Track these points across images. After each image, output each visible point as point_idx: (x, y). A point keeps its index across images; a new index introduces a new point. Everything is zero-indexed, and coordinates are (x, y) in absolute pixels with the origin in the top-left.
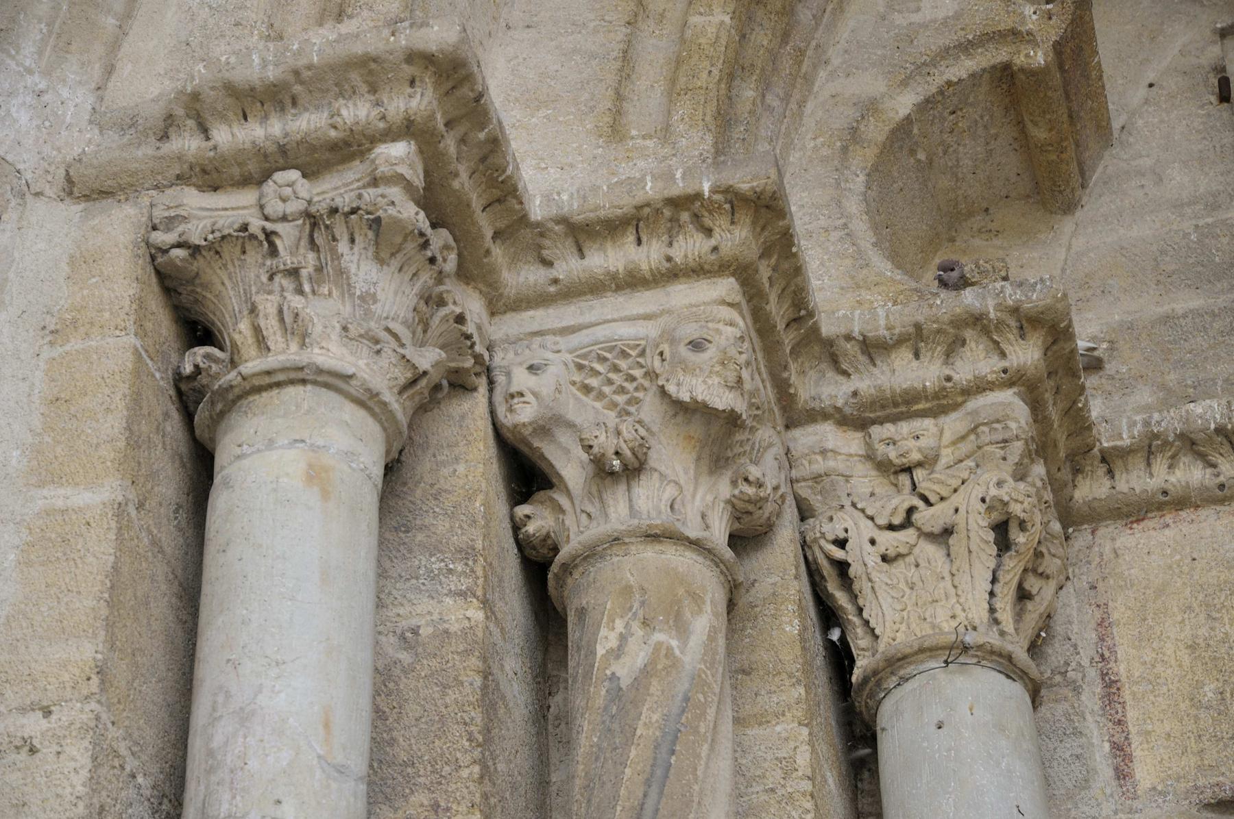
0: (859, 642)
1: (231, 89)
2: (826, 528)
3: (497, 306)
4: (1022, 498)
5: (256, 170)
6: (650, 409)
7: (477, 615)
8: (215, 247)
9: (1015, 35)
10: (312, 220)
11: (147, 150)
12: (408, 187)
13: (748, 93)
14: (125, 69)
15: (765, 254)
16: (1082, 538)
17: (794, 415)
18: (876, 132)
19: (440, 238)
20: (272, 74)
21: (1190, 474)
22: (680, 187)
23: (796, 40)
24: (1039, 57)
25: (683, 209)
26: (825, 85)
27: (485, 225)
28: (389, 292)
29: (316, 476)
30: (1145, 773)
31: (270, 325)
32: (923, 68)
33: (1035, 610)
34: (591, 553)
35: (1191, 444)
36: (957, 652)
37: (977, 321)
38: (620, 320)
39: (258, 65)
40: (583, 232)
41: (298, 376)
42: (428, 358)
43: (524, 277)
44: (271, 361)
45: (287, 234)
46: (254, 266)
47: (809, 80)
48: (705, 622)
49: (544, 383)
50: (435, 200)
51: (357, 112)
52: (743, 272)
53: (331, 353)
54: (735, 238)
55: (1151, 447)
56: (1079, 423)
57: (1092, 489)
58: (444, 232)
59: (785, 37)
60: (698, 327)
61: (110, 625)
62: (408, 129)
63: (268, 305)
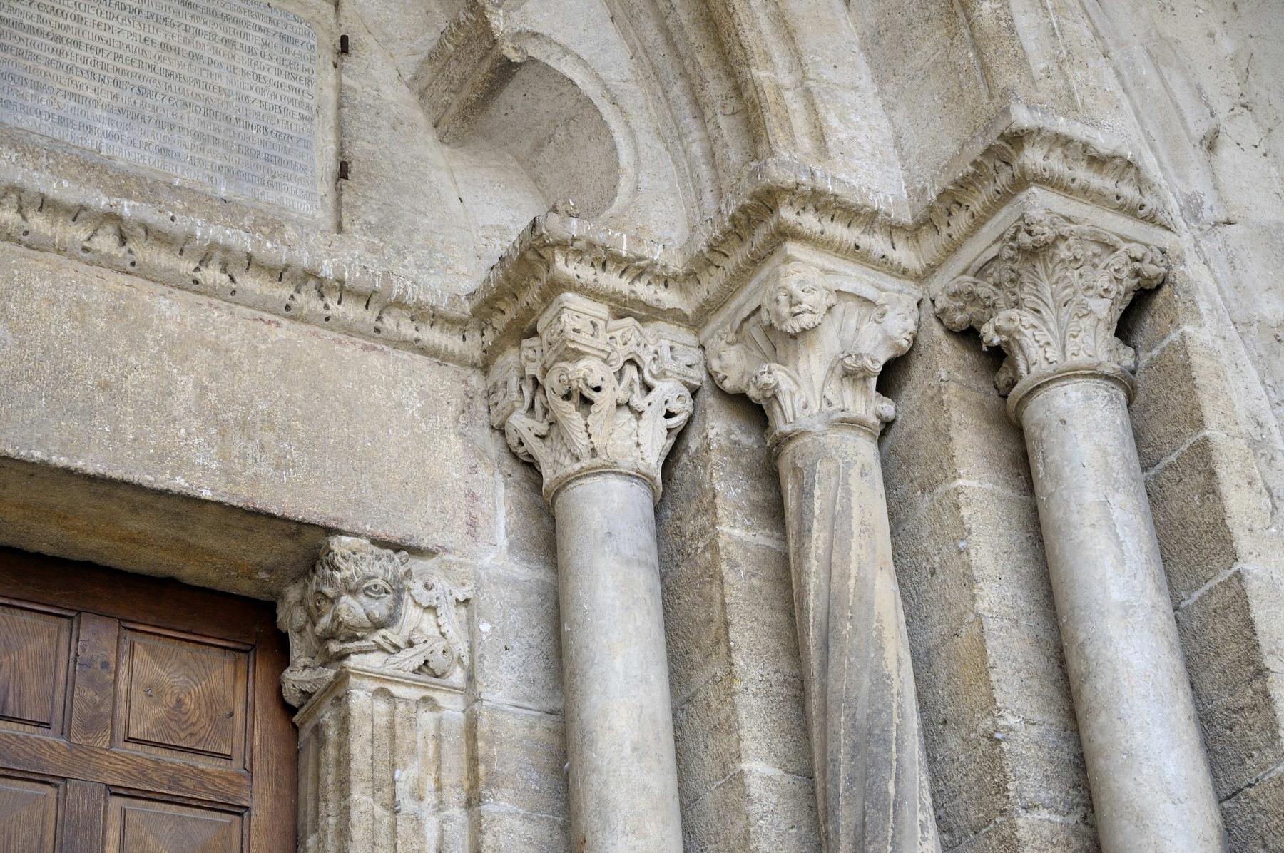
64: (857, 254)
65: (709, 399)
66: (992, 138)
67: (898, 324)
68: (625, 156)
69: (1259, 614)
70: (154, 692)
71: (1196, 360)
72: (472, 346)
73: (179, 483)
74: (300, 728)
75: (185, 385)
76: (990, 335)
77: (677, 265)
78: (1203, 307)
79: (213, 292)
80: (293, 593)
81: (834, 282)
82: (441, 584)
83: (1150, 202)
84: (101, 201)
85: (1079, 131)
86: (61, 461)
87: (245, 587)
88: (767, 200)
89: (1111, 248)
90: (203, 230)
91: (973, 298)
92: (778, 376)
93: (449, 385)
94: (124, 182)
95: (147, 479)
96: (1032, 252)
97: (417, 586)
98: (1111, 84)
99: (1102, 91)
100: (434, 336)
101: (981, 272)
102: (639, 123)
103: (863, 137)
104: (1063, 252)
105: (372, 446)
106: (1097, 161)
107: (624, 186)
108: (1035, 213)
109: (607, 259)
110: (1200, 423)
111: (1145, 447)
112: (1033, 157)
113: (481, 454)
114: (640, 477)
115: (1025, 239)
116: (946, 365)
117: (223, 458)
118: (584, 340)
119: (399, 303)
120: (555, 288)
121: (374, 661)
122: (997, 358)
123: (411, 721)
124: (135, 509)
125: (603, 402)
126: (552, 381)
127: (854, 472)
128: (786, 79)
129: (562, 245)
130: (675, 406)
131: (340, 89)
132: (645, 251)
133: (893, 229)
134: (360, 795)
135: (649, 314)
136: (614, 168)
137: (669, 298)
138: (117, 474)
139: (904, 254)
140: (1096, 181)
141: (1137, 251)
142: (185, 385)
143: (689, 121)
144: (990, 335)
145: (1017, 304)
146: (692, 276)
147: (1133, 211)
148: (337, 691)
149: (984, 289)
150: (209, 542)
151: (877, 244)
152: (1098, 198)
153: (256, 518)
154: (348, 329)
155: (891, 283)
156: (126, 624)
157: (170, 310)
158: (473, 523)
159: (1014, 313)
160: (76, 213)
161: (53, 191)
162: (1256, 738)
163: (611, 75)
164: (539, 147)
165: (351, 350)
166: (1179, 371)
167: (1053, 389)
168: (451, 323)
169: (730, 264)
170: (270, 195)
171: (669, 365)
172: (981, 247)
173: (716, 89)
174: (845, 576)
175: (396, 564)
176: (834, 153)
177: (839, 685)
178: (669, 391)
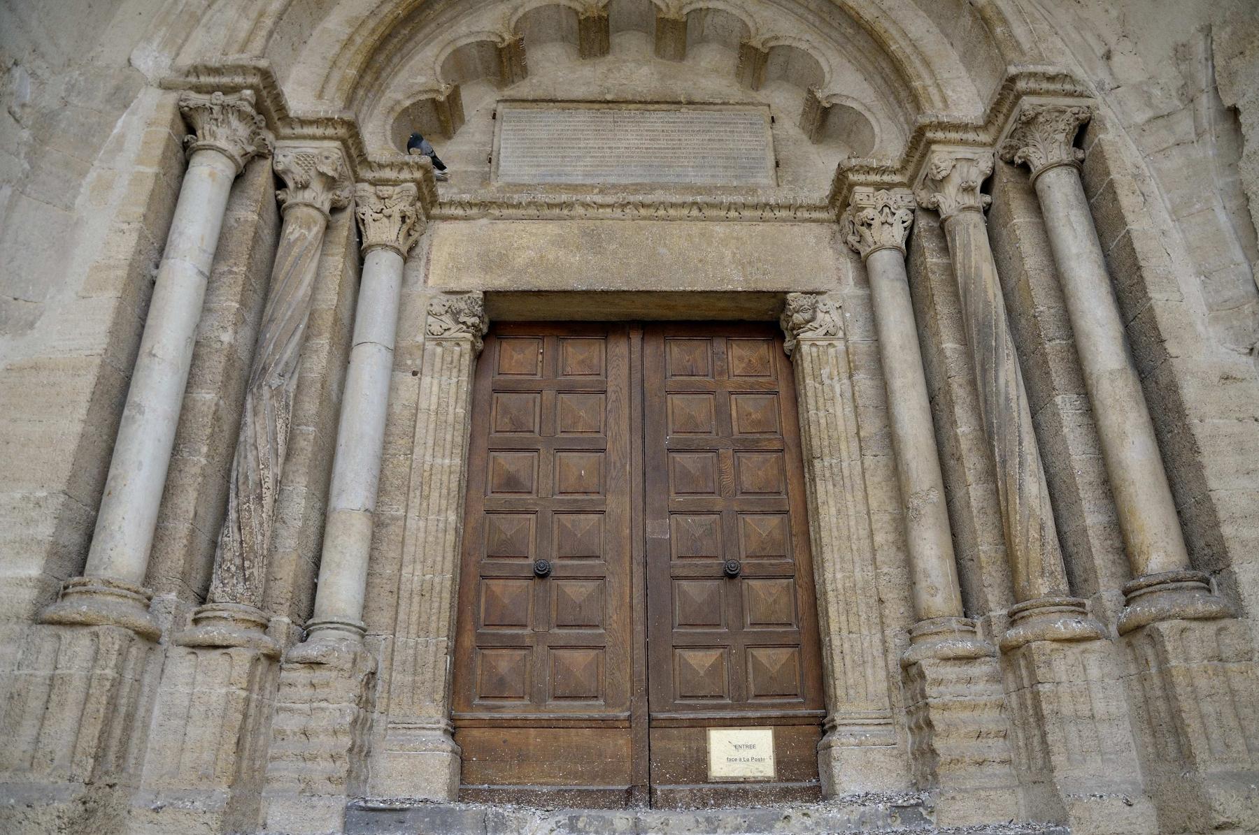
0: (364, 240)
1: (206, 67)
2: (361, 210)
3: (278, 137)
4: (410, 211)
5: (210, 90)
6: (313, 173)
7: (256, 217)
8: (197, 109)
9: (438, 91)
10: (223, 107)
11: (181, 79)
12: (250, 103)
13: (361, 92)
14: (182, 55)
15: (351, 137)
16: (431, 223)
17: (358, 180)
18: (398, 109)
19: (258, 118)
20: (217, 65)
21: (460, 212)
22: (329, 116)
23: (380, 80)
24: (442, 98)
25: (329, 121)
26: (388, 94)
27: (275, 116)
28: (242, 130)
29: (212, 175)
30: (430, 282)
31: (207, 133)
32: (413, 95)
33: (412, 239)
34: (291, 207)
35: (461, 204)
36: (385, 246)
37: (407, 164)
38: (309, 147)
39: (214, 62)
40: (303, 122)
41: (211, 148)
42: (250, 149)
43: (286, 131)
44: (206, 143)
45: (216, 109)
46: (206, 116)
47: (383, 92)
48: (317, 229)
49: (286, 160)
50: (259, 106)
51: (239, 80)
52: (344, 142)
53: (222, 143)
54: (342, 131)
55: (451, 203)
56: (434, 195)
57: (435, 211)
58: (262, 117)
59: (377, 79)
60: (328, 153)
61: (149, 205)
62: (251, 87)
63: (207, 127)
64: (962, 142)
65: (918, 213)
66: (1003, 82)
67: (985, 165)
68: (877, 130)
69: (1137, 245)
70: (741, 359)
71: (1105, 148)
72: (832, 215)
73: (730, 288)
74: (791, 360)
75: (728, 254)
76: (1018, 160)
77: (897, 165)
78: (1108, 126)
79: (734, 220)
80: (782, 317)
81: (954, 156)
82: (830, 303)
83: (1079, 88)
84: (690, 199)
85: (1040, 69)
86: (689, 289)
87: (766, 318)
88: (921, 131)
89: (1064, 112)
90: (726, 199)
91: (1011, 147)
92: (939, 197)
93: (824, 231)
94: (699, 190)
95: (719, 288)
96: (1029, 123)
97: (820, 305)
98: (1060, 44)
99: (1052, 46)
100: (815, 215)
101: (1012, 136)
102: (880, 115)
103: (962, 95)
104: (1041, 119)
105: (800, 260)
106: (1051, 79)
107: (877, 140)
108: (1026, 107)
109: (870, 170)
110: (1108, 174)
111: (1087, 189)
112: (1021, 85)
113: (840, 253)
114: (897, 248)
115: (1023, 118)
116: (1006, 177)
117: (745, 276)
118: (865, 203)
119: (801, 206)
120: (851, 186)
121: (809, 334)
122: (1025, 168)
123: (826, 353)
124: (719, 300)
125: (876, 223)
126: (856, 220)
127: (971, 227)
128: (929, 82)
129: (850, 169)
130: (905, 218)
131: (773, 136)
132: (884, 163)
133: (976, 129)
134: (809, 381)
135: (890, 186)
136: (873, 135)
137: (897, 178)
138: (708, 289)
139: (984, 137)
140: (1052, 87)
141: (1076, 110)
142: (728, 254)
143: (898, 109)
144: (1018, 160)
145: (1027, 145)
146: (903, 168)
147: (1071, 94)
148: (798, 346)
149: (1014, 142)
150: (747, 305)
151: (971, 136)
152: (1055, 93)
153: (759, 294)
154: (784, 220)
155: (980, 150)
156: (728, 338)
157: (719, 229)
158: (839, 279)
159: (1025, 149)
160: (683, 205)
161: (674, 200)
162: (1139, 295)
163: (867, 101)
164: (849, 136)
165: (786, 227)
166: (1099, 155)
167: (1044, 175)
168: (822, 208)
169: (915, 160)
170: (752, 180)
171: (901, 203)
172: (1009, 127)
173: (903, 94)
174: (970, 267)
175: (812, 299)
176: (951, 105)
177: (971, 309)
178: (902, 213)
